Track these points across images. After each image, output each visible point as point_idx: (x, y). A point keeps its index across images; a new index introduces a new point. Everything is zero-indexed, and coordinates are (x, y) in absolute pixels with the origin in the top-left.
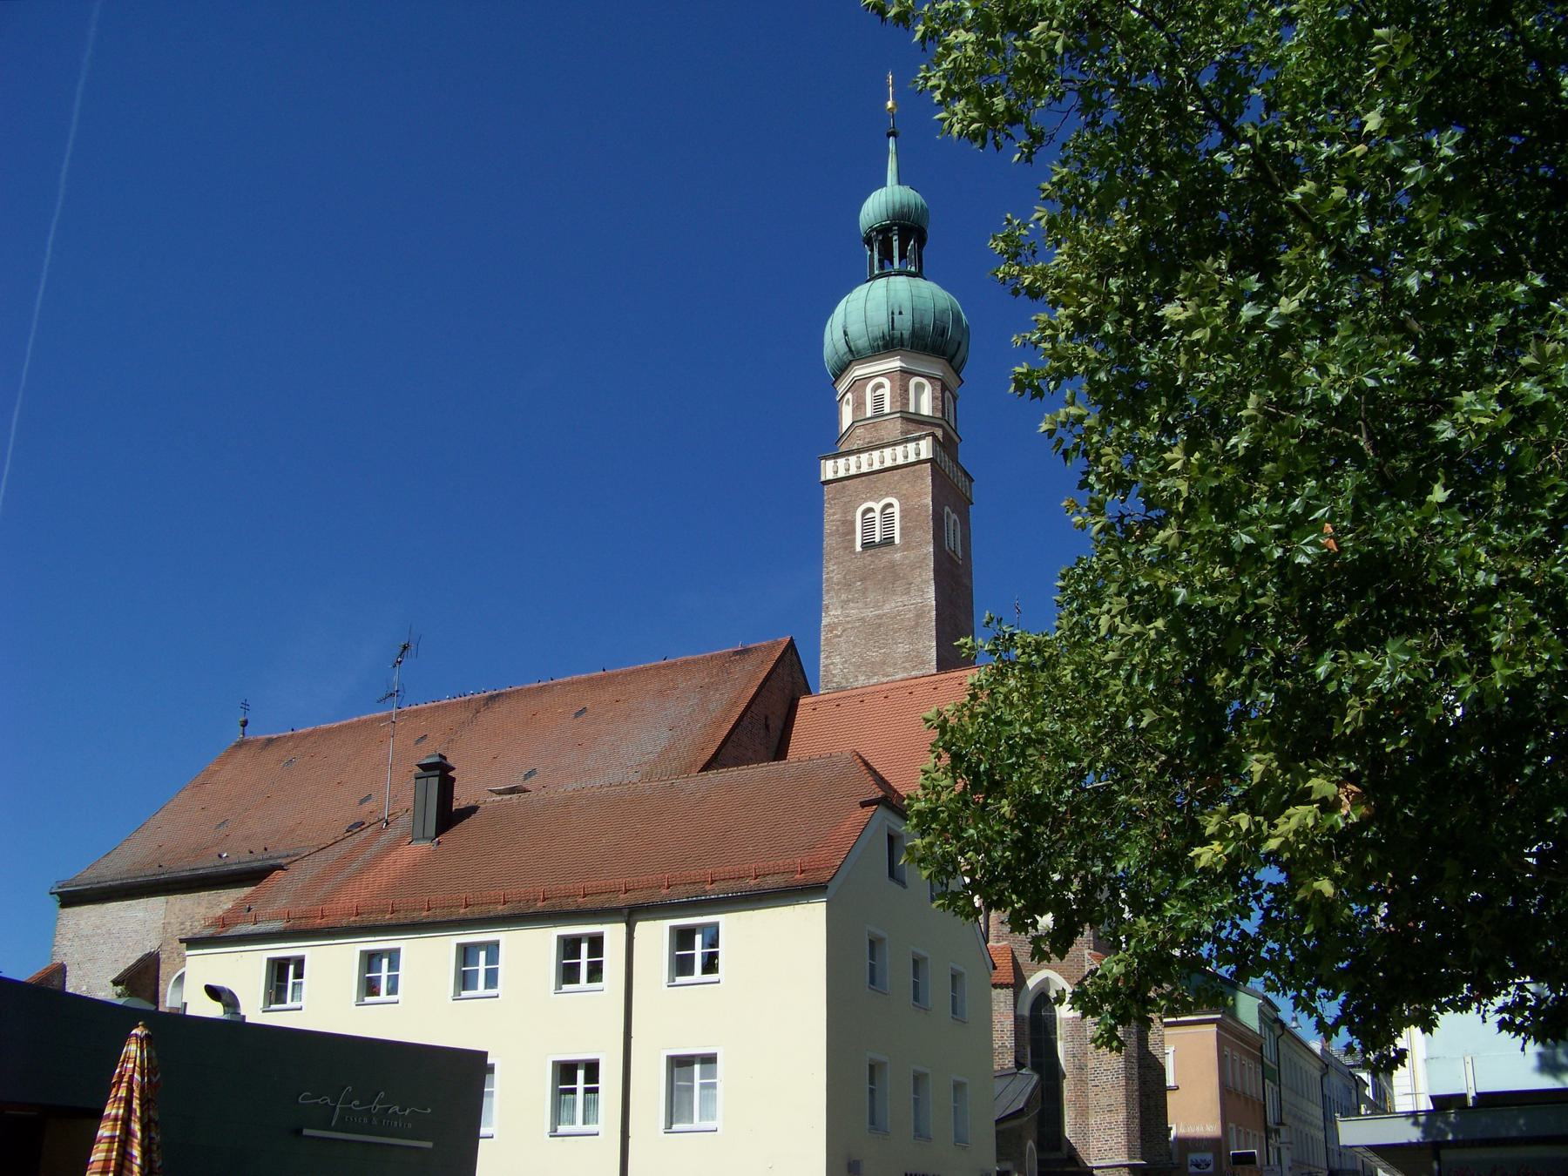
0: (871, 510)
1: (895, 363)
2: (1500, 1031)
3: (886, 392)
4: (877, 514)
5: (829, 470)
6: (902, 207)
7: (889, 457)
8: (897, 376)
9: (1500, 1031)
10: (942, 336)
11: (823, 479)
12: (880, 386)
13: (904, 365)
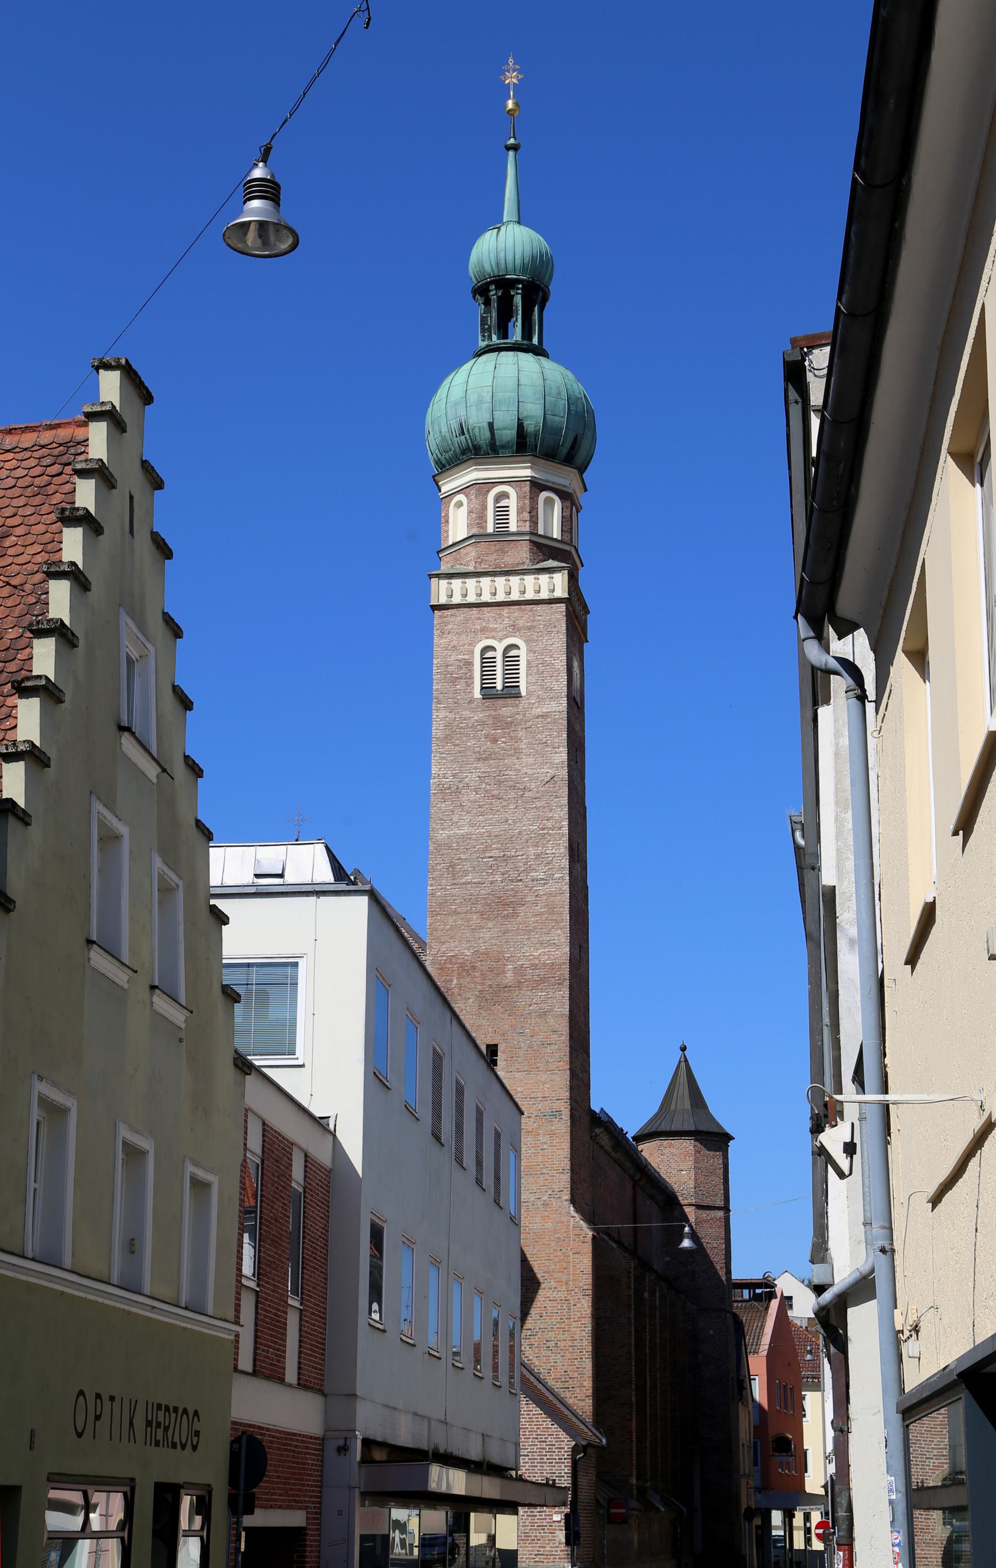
0: (492, 648)
1: (524, 472)
2: (822, 1487)
3: (512, 503)
4: (499, 655)
5: (442, 591)
6: (533, 258)
7: (500, 588)
8: (527, 488)
9: (822, 1487)
10: (463, 434)
11: (434, 602)
12: (504, 495)
13: (535, 475)
